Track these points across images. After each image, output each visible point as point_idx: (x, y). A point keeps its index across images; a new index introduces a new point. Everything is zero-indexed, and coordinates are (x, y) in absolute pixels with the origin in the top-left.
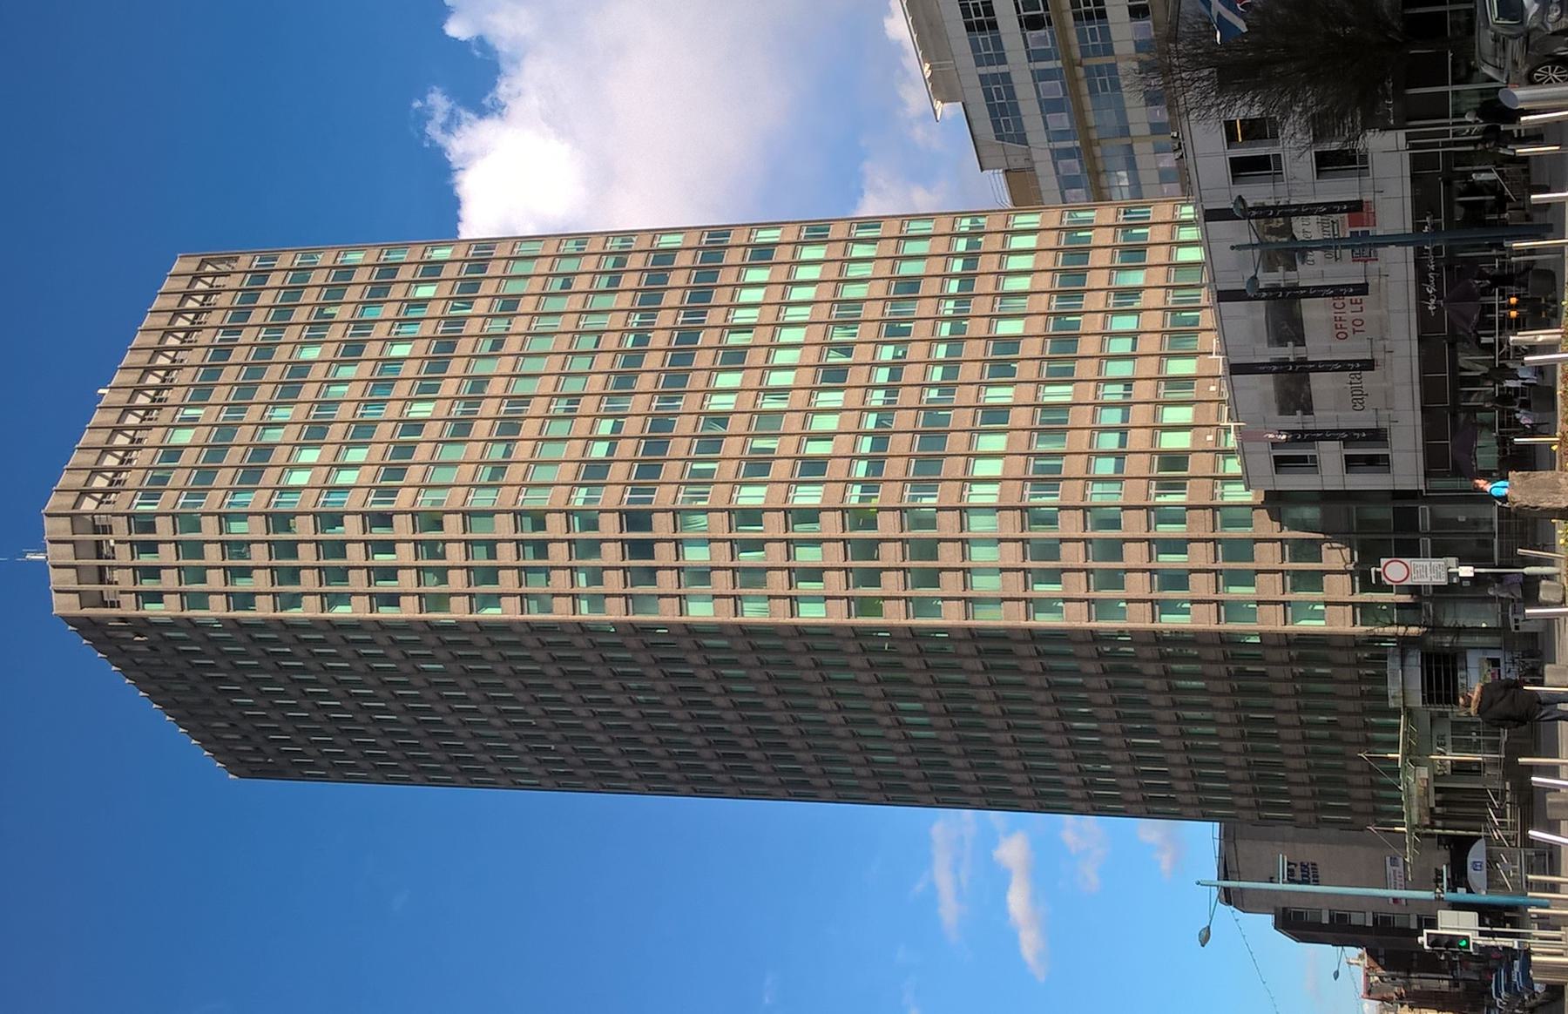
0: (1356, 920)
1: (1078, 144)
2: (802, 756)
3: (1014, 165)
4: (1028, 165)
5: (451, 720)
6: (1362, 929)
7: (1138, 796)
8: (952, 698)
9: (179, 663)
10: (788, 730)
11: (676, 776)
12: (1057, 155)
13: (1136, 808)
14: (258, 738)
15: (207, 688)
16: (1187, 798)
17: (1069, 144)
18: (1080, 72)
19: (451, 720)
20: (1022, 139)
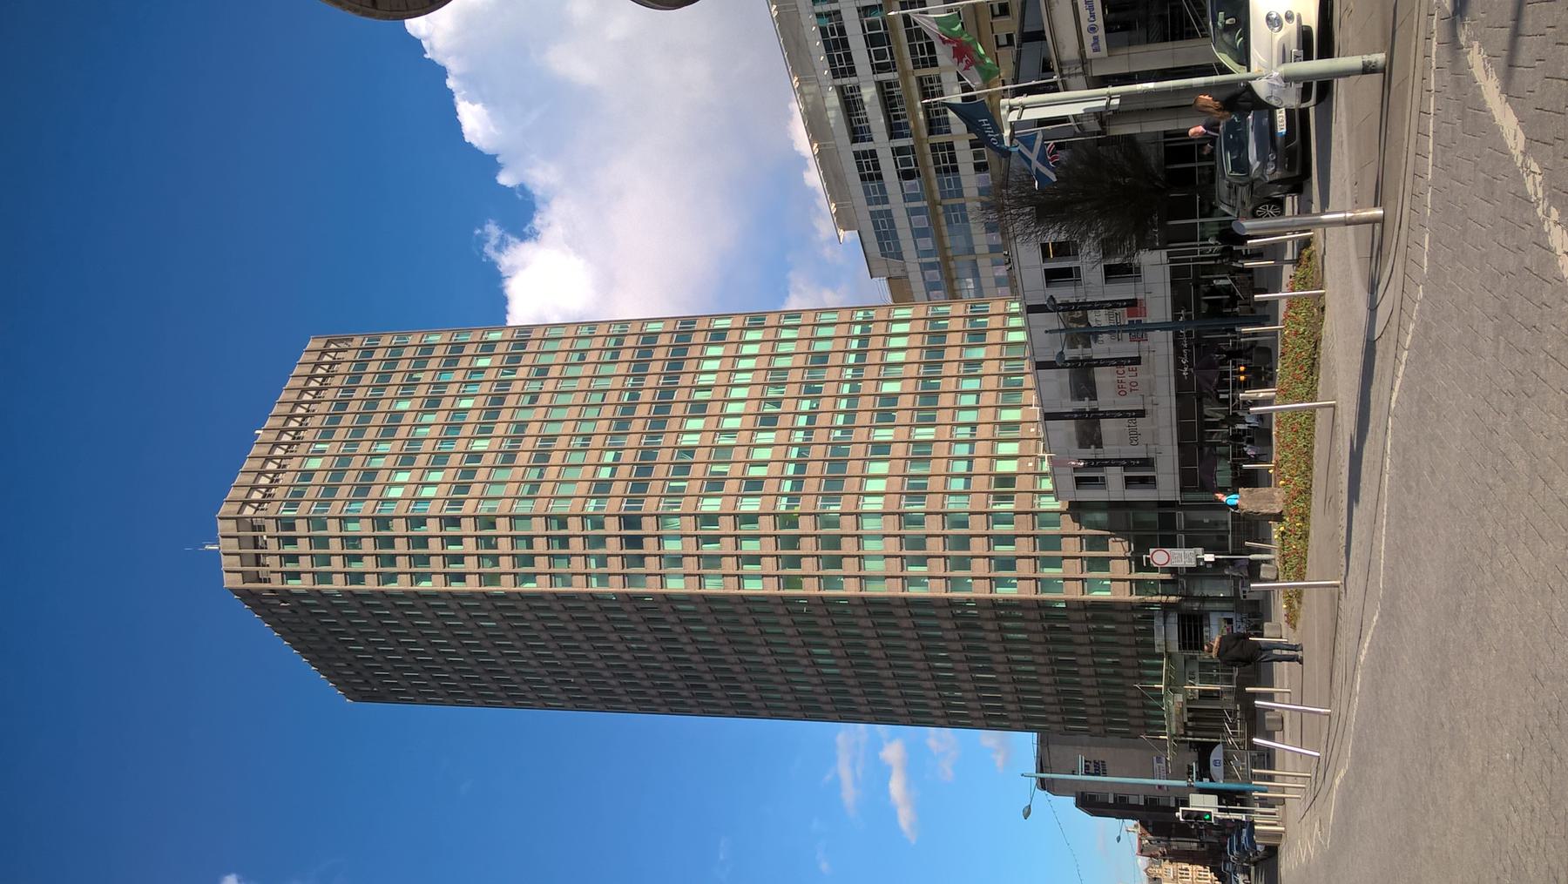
0: (1133, 800)
3: (894, 274)
6: (1137, 807)
12: (925, 267)
20: (900, 256)
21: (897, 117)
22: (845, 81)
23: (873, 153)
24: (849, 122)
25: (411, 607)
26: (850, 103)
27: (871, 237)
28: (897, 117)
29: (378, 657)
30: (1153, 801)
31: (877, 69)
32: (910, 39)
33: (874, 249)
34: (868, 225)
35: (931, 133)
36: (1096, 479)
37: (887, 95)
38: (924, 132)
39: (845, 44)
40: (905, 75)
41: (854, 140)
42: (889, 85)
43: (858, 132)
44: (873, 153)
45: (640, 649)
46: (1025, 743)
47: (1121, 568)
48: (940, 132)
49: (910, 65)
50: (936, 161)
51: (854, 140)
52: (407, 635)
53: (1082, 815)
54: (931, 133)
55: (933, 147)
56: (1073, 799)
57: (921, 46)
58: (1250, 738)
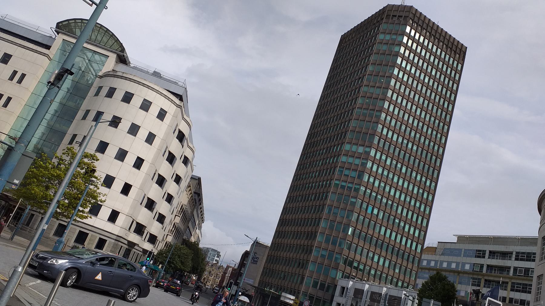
0: (243, 269)
1: (484, 272)
2: (303, 171)
3: (437, 250)
4: (437, 253)
5: (339, 86)
6: (240, 270)
7: (292, 195)
8: (302, 209)
9: (369, 29)
10: (319, 147)
11: (313, 132)
12: (436, 262)
13: (274, 241)
14: (348, 43)
15: (362, 34)
16: (289, 205)
17: (460, 267)
18: (480, 277)
19: (339, 86)
20: (443, 254)
21: (495, 270)
22: (514, 256)
23: (484, 257)
24: (498, 252)
25: (364, 62)
26: (505, 255)
27: (453, 246)
28: (495, 270)
29: (366, 39)
30: (241, 275)
31: (515, 269)
32: (523, 284)
33: (448, 246)
34: (457, 246)
35: (486, 280)
36: (343, 294)
37: (504, 269)
38: (486, 278)
39: (527, 260)
40: (511, 278)
41: (490, 252)
42: (508, 271)
43: (493, 254)
44: (484, 257)
45: (320, 133)
46: (267, 240)
47: (311, 291)
48: (485, 284)
49: (513, 281)
50: (518, 284)
51: (490, 252)
52: (356, 59)
53: (243, 252)
54: (486, 280)
55: (480, 279)
56: (249, 250)
57: (520, 287)
58: (146, 266)
